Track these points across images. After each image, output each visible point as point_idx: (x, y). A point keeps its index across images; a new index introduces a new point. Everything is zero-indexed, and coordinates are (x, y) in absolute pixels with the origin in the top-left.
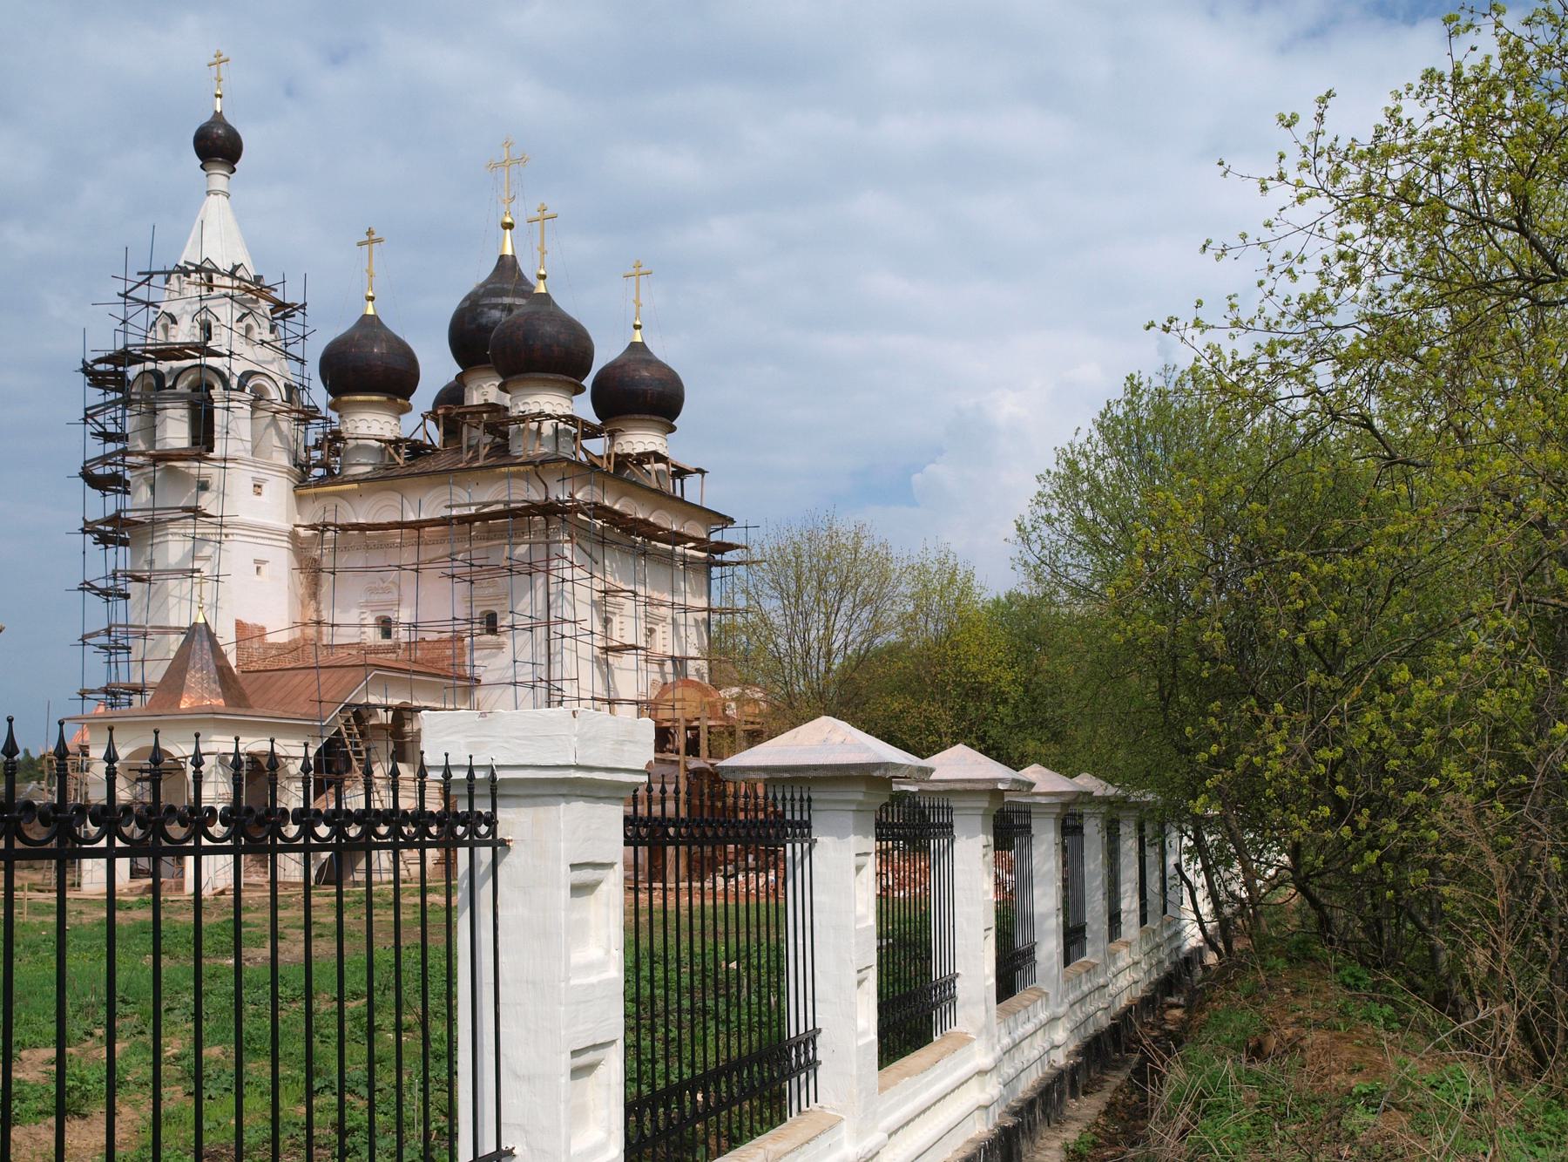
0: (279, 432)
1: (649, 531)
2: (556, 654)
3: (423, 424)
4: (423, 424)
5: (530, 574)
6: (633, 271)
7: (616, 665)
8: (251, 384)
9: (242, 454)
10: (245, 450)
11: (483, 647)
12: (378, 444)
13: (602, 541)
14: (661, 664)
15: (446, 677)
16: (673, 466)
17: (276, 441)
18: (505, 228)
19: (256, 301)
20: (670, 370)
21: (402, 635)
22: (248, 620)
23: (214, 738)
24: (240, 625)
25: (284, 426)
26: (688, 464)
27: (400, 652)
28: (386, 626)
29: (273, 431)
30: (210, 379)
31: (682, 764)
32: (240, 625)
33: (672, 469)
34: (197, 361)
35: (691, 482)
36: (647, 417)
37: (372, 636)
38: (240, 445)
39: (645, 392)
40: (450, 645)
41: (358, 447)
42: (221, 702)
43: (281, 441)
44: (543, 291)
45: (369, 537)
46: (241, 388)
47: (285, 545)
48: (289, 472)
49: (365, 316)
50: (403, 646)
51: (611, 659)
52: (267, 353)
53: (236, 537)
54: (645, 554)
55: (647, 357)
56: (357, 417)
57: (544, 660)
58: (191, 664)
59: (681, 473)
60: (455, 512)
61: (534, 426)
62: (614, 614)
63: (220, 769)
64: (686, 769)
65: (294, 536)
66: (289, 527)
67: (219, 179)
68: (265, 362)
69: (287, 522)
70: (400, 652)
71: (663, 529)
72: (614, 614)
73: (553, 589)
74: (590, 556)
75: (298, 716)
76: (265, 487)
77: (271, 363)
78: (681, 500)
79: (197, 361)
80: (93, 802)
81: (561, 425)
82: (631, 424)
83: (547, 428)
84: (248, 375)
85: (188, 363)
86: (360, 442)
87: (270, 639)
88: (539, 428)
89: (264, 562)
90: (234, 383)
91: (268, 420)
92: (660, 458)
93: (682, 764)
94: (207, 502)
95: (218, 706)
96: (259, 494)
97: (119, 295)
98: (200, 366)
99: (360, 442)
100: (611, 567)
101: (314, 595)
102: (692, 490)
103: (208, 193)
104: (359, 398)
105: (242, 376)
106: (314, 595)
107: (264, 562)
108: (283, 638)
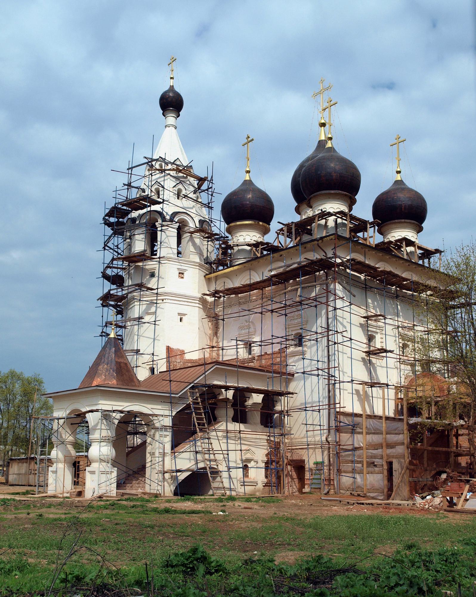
0: (194, 244)
1: (399, 282)
2: (332, 355)
3: (278, 237)
4: (278, 237)
5: (316, 306)
6: (396, 141)
7: (378, 364)
8: (176, 219)
9: (172, 256)
10: (173, 253)
11: (294, 354)
12: (248, 248)
13: (366, 287)
14: (413, 365)
15: (268, 372)
16: (420, 248)
17: (192, 249)
18: (321, 126)
19: (186, 178)
20: (416, 192)
21: (256, 350)
22: (174, 346)
23: (101, 402)
24: (168, 349)
25: (197, 241)
26: (431, 247)
27: (255, 361)
28: (249, 345)
29: (190, 244)
30: (156, 217)
31: (405, 420)
32: (168, 349)
33: (419, 252)
34: (149, 209)
35: (435, 258)
36: (403, 220)
37: (243, 354)
38: (170, 251)
39: (400, 206)
40: (279, 355)
41: (239, 251)
42: (115, 382)
43: (195, 249)
44: (330, 146)
45: (241, 298)
46: (171, 220)
47: (197, 305)
48: (200, 265)
49: (245, 181)
50: (256, 358)
51: (374, 360)
52: (191, 204)
53: (167, 301)
54: (397, 297)
55: (403, 186)
56: (238, 235)
57: (326, 360)
58: (103, 361)
59: (427, 254)
60: (273, 273)
61: (323, 222)
62: (377, 333)
63: (104, 421)
64: (408, 424)
65: (203, 301)
66: (199, 295)
67: (171, 119)
68: (188, 208)
69: (199, 293)
70: (255, 361)
71: (406, 280)
72: (377, 333)
73: (331, 315)
74: (349, 291)
75: (290, 421)
76: (186, 274)
77: (192, 208)
78: (429, 268)
79: (149, 209)
80: (114, 451)
81: (339, 221)
82: (393, 226)
83: (331, 222)
84: (175, 214)
85: (145, 210)
86: (240, 248)
87: (188, 357)
88: (326, 223)
89: (185, 315)
90: (168, 217)
91: (188, 238)
92: (410, 243)
93: (405, 420)
94: (152, 283)
95: (113, 384)
96: (182, 278)
97: (125, 185)
98: (150, 211)
99: (240, 248)
100: (373, 303)
101: (216, 334)
102: (435, 262)
103: (166, 127)
104: (238, 223)
105: (172, 214)
106: (216, 334)
107: (185, 315)
108: (195, 356)
